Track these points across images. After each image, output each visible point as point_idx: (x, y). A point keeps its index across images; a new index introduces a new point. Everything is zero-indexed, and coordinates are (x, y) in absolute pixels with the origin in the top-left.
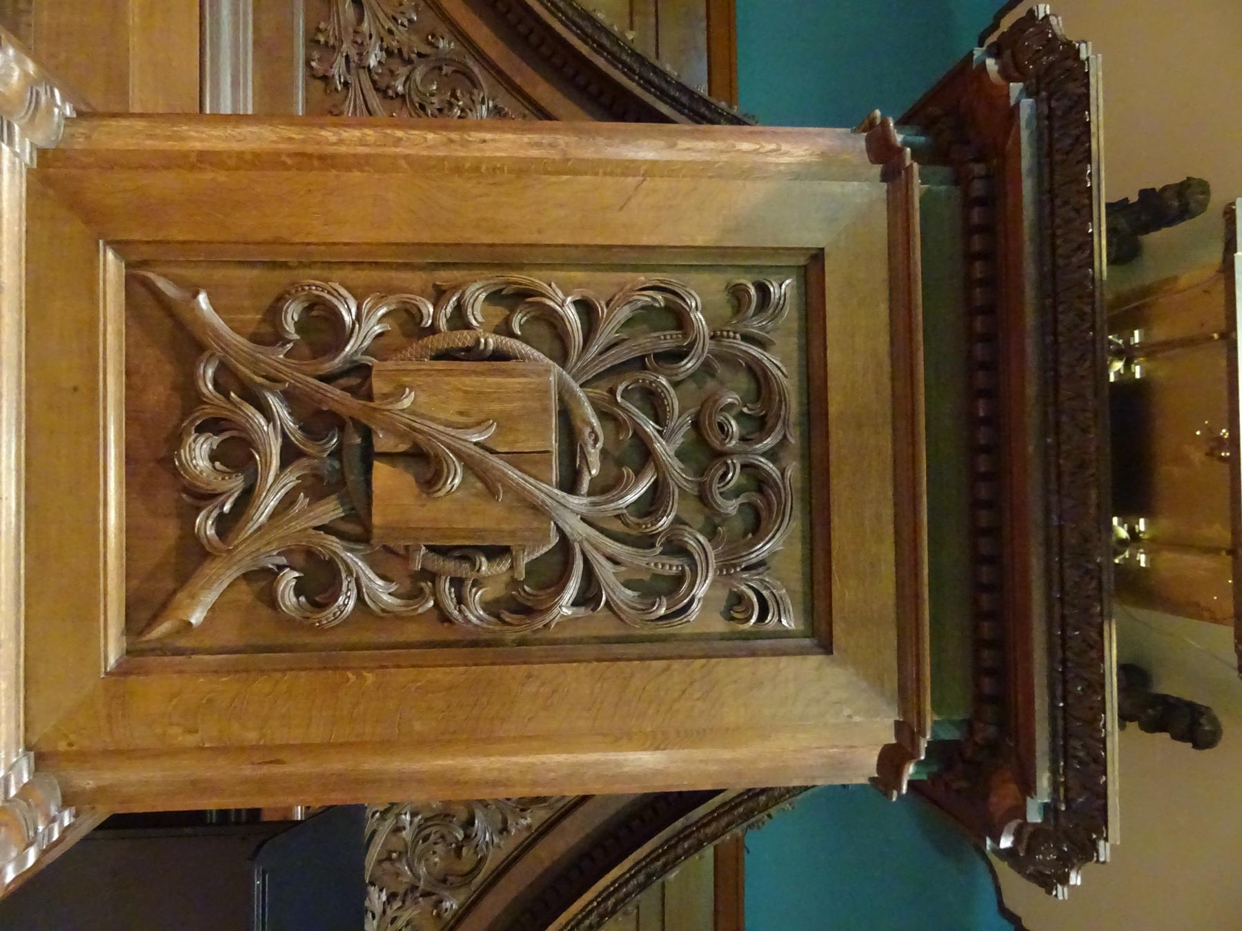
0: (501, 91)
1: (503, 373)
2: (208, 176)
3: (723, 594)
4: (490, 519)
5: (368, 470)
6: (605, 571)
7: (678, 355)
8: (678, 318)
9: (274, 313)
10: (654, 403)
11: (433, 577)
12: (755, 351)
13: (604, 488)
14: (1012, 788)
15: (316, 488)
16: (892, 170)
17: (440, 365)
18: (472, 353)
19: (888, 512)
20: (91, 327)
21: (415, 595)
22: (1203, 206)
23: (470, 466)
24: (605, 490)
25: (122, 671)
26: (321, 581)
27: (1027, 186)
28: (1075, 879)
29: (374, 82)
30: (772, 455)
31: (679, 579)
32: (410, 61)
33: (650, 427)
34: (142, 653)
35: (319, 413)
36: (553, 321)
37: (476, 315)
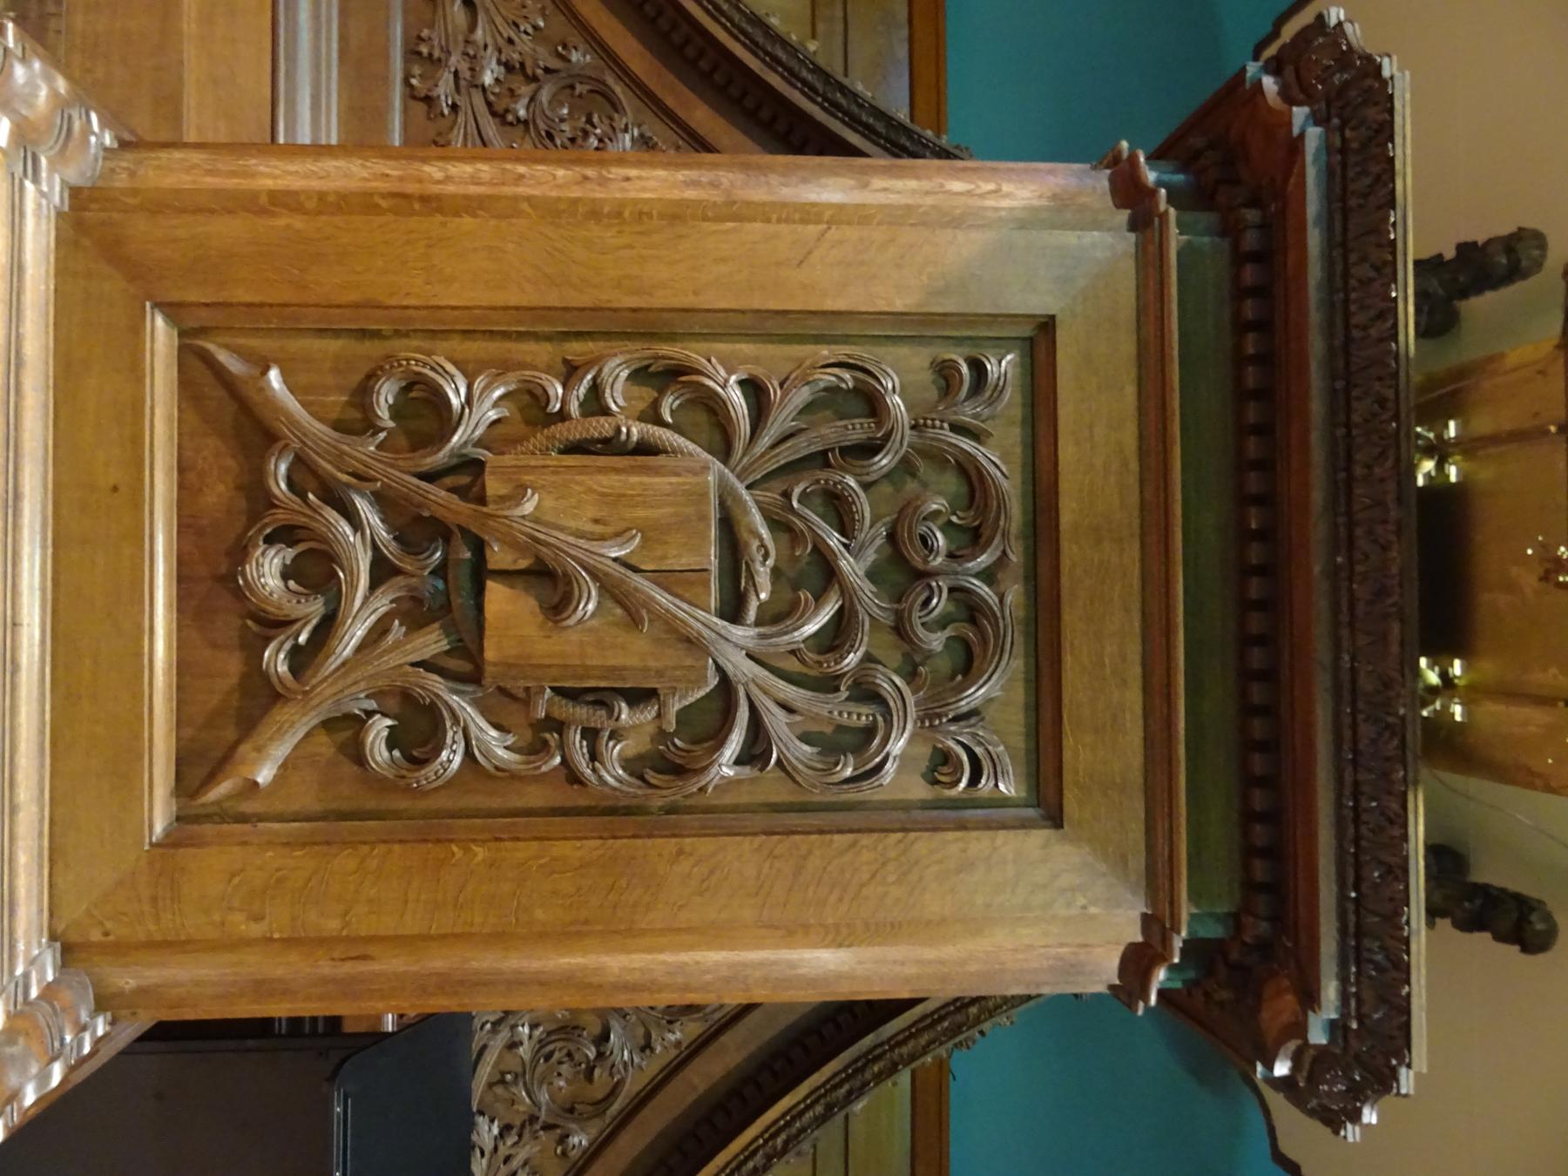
3: (924, 751)
4: (634, 655)
5: (479, 591)
6: (777, 721)
7: (870, 449)
8: (871, 402)
9: (363, 394)
10: (839, 510)
11: (560, 726)
12: (966, 444)
13: (779, 616)
15: (415, 614)
16: (1143, 220)
17: (570, 460)
18: (610, 446)
20: (134, 411)
21: (537, 749)
22: (1538, 265)
23: (611, 591)
24: (777, 619)
25: (172, 842)
26: (420, 730)
28: (1370, 1116)
29: (489, 104)
30: (988, 576)
31: (869, 732)
32: (535, 79)
33: (834, 540)
36: (713, 406)
37: (615, 398)
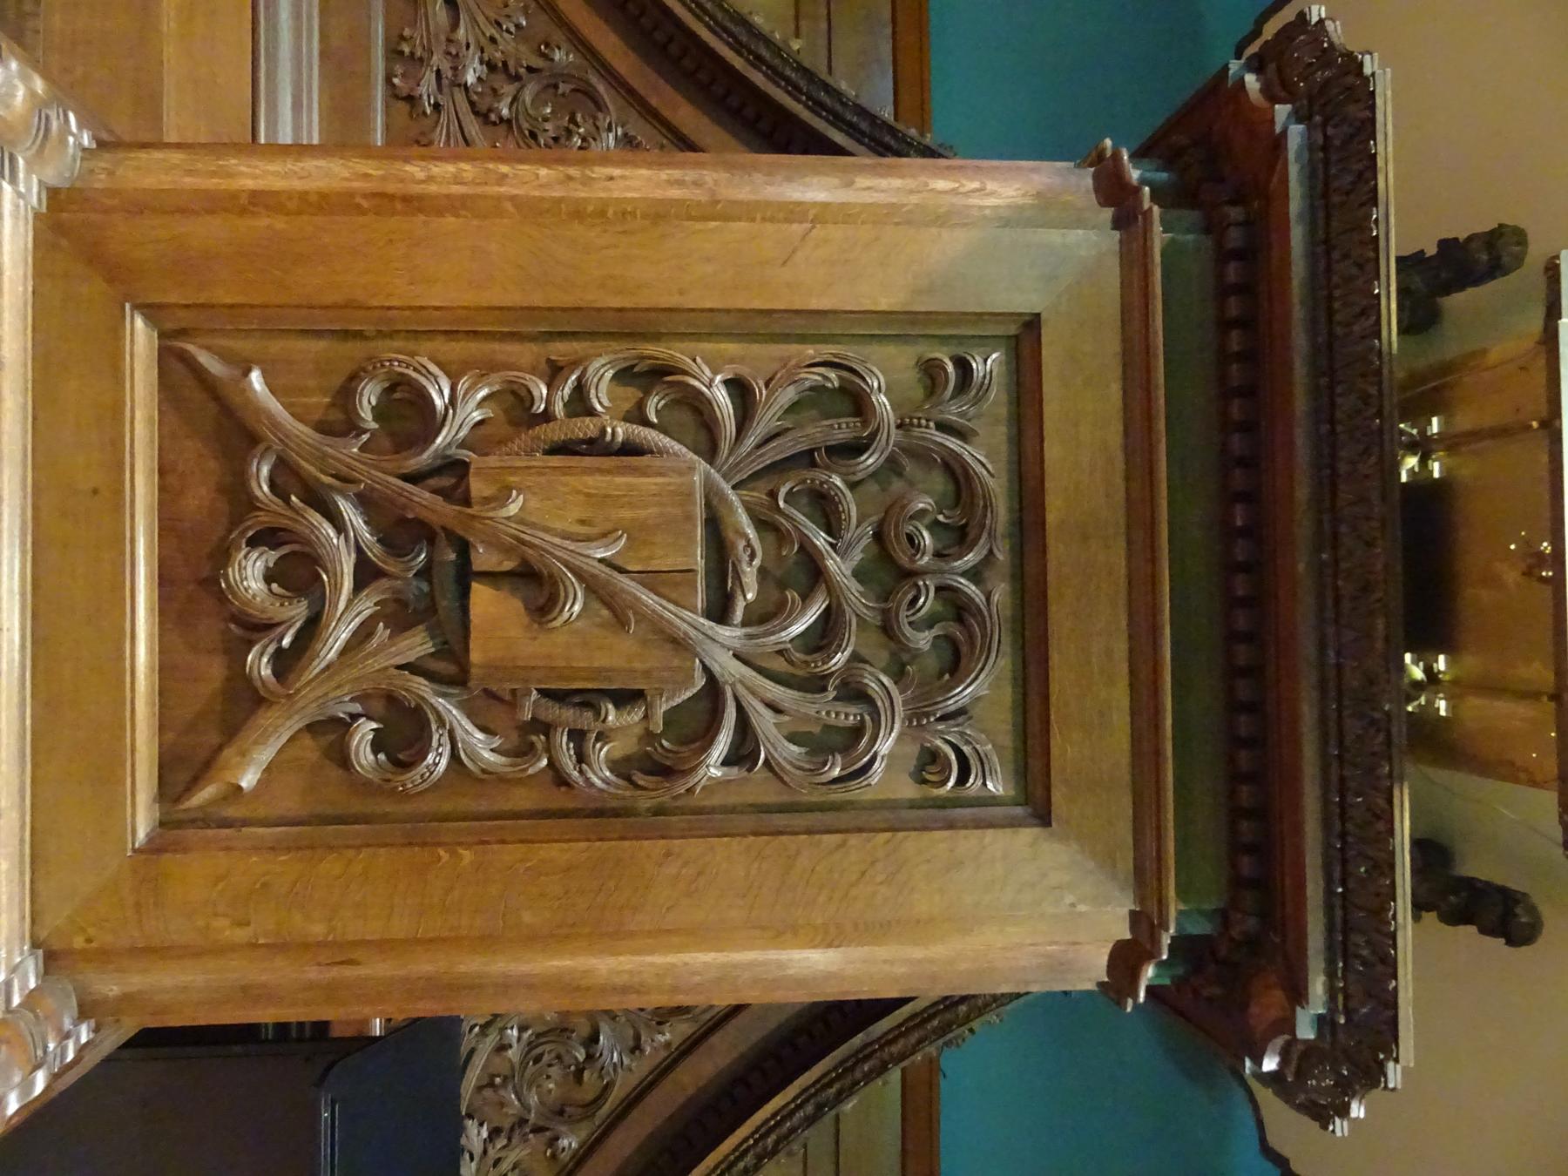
0: (633, 116)
1: (635, 471)
2: (263, 222)
3: (913, 750)
4: (619, 656)
5: (464, 594)
6: (764, 721)
7: (855, 449)
8: (856, 401)
9: (346, 395)
10: (825, 509)
11: (547, 729)
12: (953, 443)
13: (762, 617)
14: (1278, 995)
15: (399, 616)
16: (1126, 214)
17: (556, 461)
18: (596, 446)
19: (1121, 647)
20: (114, 413)
21: (524, 752)
22: (1519, 260)
23: (594, 588)
24: (764, 619)
25: (155, 848)
26: (405, 733)
27: (1297, 235)
28: (1357, 1110)
29: (472, 104)
30: (974, 574)
31: (857, 732)
32: (517, 78)
33: (821, 540)
34: (179, 824)
35: (403, 521)
36: (698, 406)
37: (600, 398)
